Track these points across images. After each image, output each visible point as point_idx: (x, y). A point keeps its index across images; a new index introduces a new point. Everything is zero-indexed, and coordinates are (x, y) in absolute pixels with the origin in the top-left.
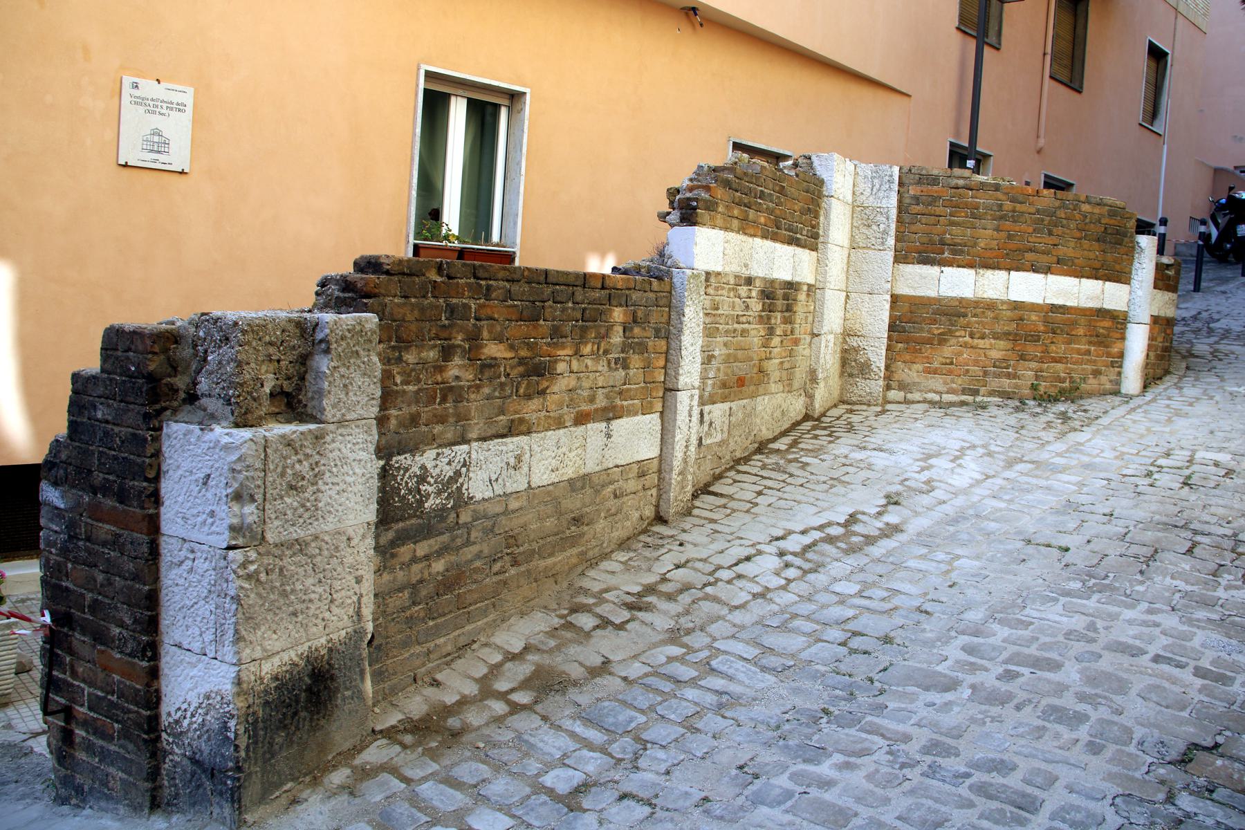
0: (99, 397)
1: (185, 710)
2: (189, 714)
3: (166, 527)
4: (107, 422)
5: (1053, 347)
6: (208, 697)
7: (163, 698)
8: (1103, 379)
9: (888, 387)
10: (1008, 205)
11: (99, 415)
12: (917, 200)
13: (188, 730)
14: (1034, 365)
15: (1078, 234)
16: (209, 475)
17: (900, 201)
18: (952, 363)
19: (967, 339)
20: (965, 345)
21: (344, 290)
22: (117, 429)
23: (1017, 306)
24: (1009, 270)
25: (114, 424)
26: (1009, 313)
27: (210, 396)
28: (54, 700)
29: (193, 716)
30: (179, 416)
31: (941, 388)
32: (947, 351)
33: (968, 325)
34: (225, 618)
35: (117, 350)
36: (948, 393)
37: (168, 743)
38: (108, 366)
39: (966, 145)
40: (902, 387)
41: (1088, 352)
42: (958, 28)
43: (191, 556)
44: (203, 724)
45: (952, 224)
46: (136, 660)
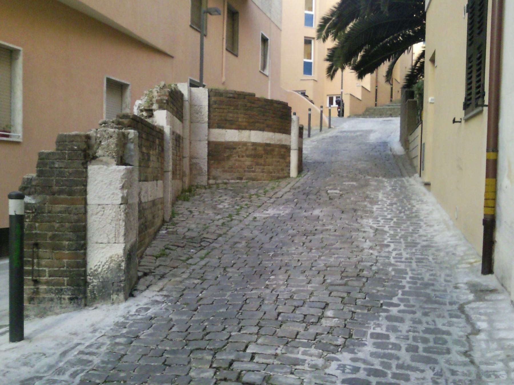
0: (56, 159)
1: (100, 265)
2: (101, 266)
3: (89, 201)
4: (61, 168)
5: (267, 160)
6: (111, 257)
7: (88, 263)
8: (285, 172)
9: (209, 179)
10: (249, 104)
11: (57, 166)
12: (215, 102)
13: (101, 272)
14: (262, 167)
15: (273, 115)
16: (111, 181)
17: (209, 103)
18: (232, 168)
19: (237, 158)
20: (236, 160)
21: (117, 125)
22: (66, 170)
23: (254, 144)
24: (250, 130)
25: (65, 168)
26: (251, 147)
27: (104, 156)
28: (27, 279)
29: (103, 266)
30: (92, 163)
31: (229, 178)
32: (230, 163)
33: (237, 152)
34: (120, 228)
35: (66, 142)
36: (232, 179)
37: (90, 279)
38: (60, 148)
39: (199, 81)
40: (215, 178)
41: (278, 162)
42: (191, 26)
43: (103, 210)
44: (109, 267)
45: (229, 112)
46: (78, 251)
